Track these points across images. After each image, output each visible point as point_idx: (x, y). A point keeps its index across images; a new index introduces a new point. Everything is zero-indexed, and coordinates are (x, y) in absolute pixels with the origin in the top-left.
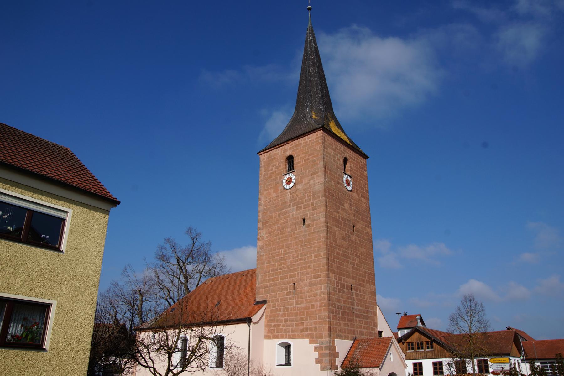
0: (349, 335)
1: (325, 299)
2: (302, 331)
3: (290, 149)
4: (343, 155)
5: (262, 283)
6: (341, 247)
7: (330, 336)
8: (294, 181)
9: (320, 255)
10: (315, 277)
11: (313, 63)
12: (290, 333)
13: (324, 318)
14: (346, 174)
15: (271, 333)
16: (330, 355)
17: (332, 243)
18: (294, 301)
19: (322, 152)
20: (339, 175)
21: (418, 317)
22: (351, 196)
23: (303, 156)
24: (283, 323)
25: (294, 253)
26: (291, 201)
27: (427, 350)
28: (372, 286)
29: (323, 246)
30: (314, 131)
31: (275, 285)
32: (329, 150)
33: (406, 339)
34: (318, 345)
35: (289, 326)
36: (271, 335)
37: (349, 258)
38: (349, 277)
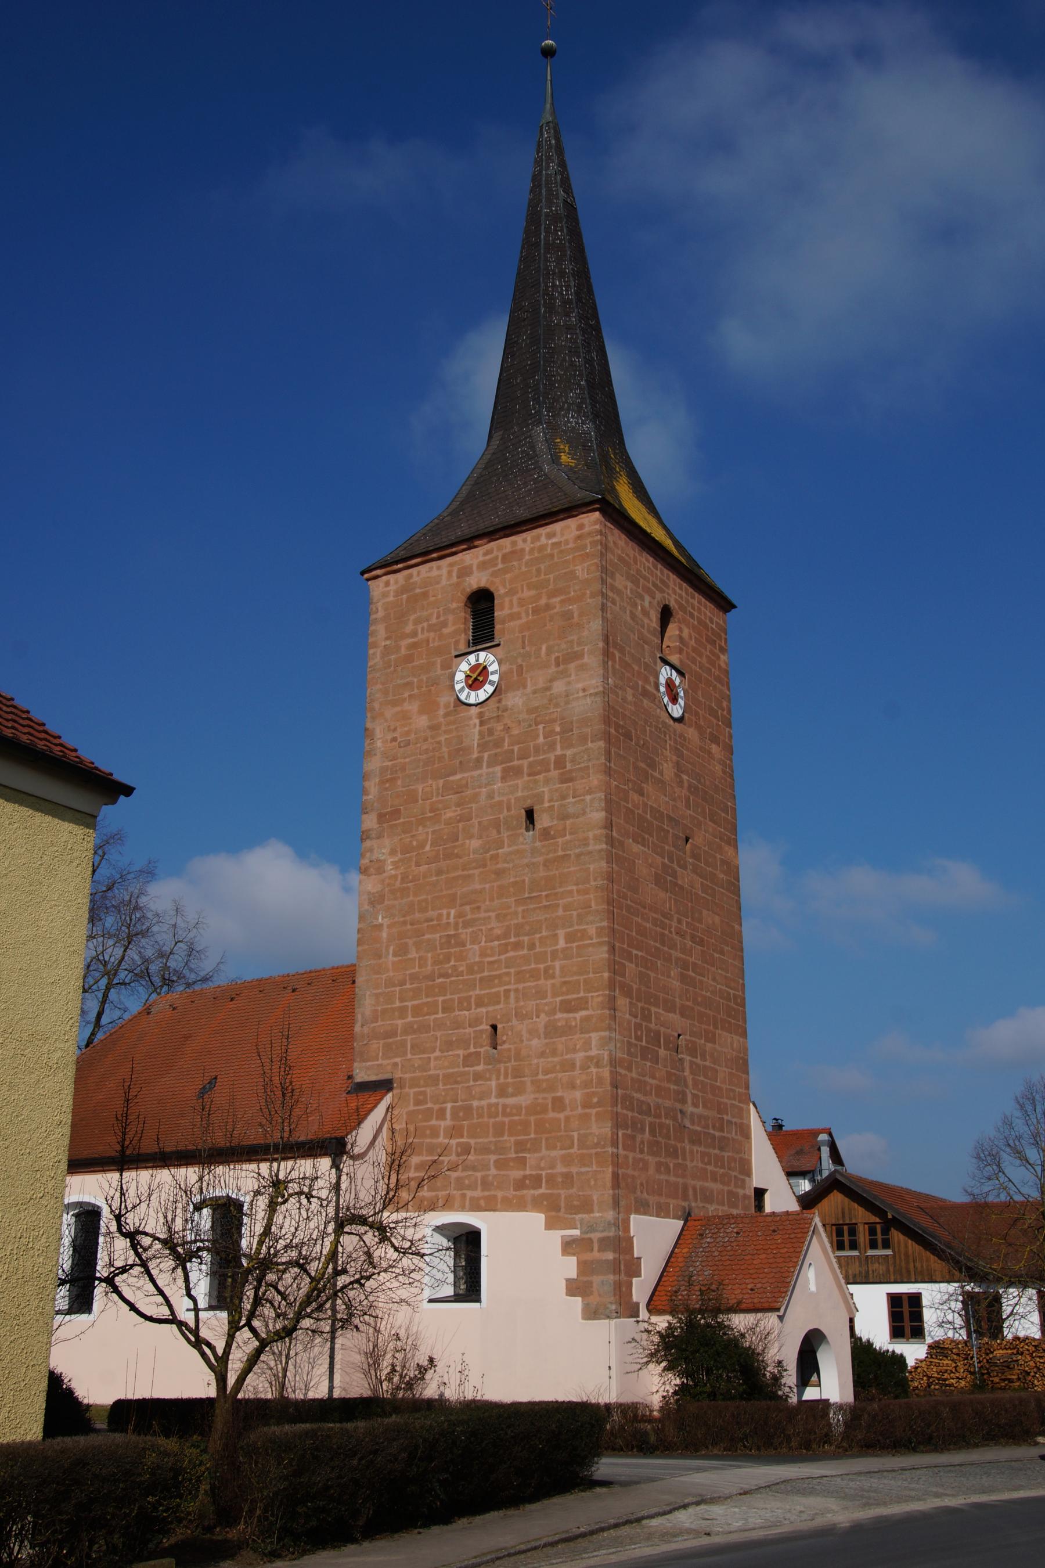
0: (672, 1202)
2: (520, 1185)
3: (483, 566)
4: (658, 596)
5: (375, 1019)
7: (616, 1203)
9: (584, 935)
10: (568, 1007)
11: (559, 261)
12: (478, 1193)
13: (597, 1145)
14: (666, 662)
16: (615, 1267)
18: (494, 1083)
19: (597, 586)
21: (823, 1137)
22: (681, 736)
23: (528, 594)
25: (494, 924)
26: (483, 747)
27: (870, 1253)
30: (570, 511)
31: (425, 1028)
32: (620, 582)
35: (474, 1168)
38: (671, 1009)
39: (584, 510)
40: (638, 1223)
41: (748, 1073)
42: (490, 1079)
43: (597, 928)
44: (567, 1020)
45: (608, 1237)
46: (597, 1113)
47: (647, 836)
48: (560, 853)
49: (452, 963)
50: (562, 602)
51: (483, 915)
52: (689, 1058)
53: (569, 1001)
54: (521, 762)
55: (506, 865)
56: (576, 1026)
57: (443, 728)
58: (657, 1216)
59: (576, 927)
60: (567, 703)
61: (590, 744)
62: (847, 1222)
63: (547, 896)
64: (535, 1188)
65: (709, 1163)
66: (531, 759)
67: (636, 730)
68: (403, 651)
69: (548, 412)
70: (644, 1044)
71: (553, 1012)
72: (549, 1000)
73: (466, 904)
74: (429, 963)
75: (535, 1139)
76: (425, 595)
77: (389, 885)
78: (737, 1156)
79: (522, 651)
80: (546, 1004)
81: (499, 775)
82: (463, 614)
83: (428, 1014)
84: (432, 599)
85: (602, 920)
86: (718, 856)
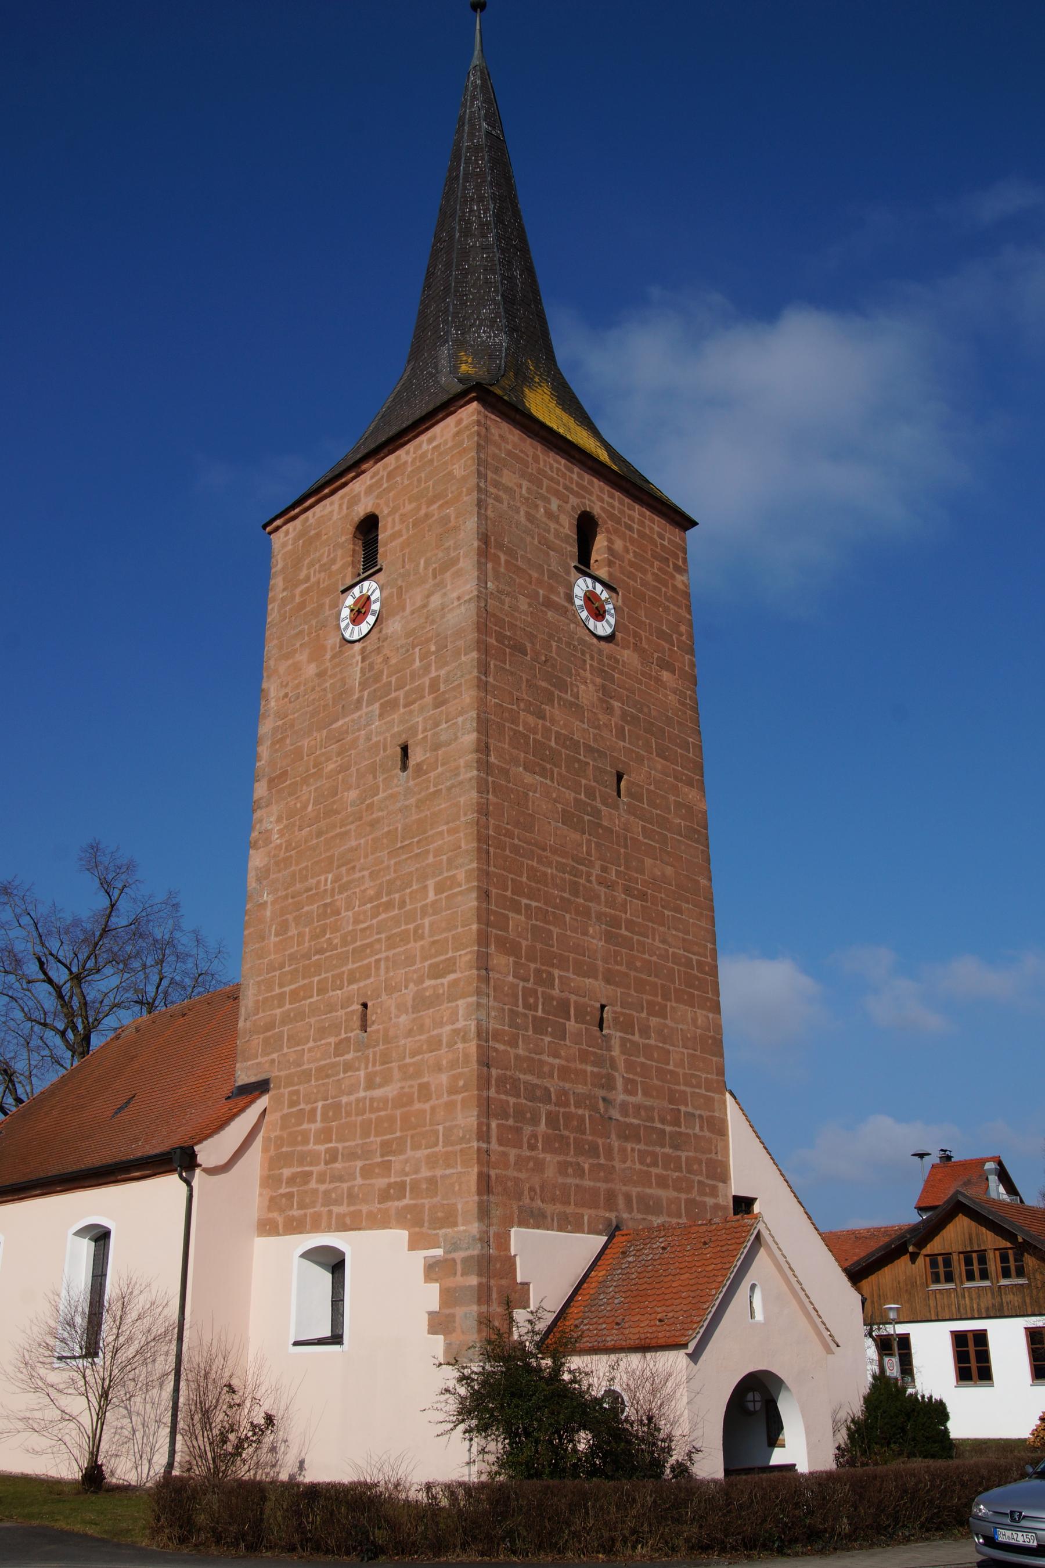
0: (587, 1214)
1: (466, 1056)
2: (385, 1196)
4: (573, 500)
6: (554, 851)
7: (484, 1213)
8: (376, 607)
9: (453, 881)
10: (437, 972)
11: (478, 187)
13: (462, 1140)
15: (281, 1210)
17: (509, 834)
18: (362, 1073)
19: (473, 481)
20: (553, 575)
21: (990, 1165)
23: (409, 507)
24: (322, 1167)
26: (364, 685)
27: (1004, 1282)
28: (702, 1015)
29: (468, 844)
31: (300, 1015)
32: (508, 478)
33: (921, 1244)
34: (439, 1252)
35: (341, 1179)
36: (280, 1220)
37: (596, 898)
39: (462, 402)
40: (522, 1241)
41: (722, 1056)
42: (358, 1069)
43: (466, 872)
44: (435, 987)
45: (472, 1257)
46: (463, 1100)
47: (548, 766)
48: (432, 790)
49: (328, 936)
50: (441, 507)
51: (357, 875)
52: (619, 1034)
53: (437, 965)
54: (397, 693)
55: (380, 814)
56: (443, 994)
57: (329, 673)
58: (560, 1229)
59: (446, 875)
60: (443, 617)
61: (463, 658)
62: (976, 1248)
63: (418, 842)
64: (399, 1199)
65: (655, 1164)
66: (407, 688)
67: (533, 644)
68: (298, 599)
69: (457, 330)
70: (540, 1013)
71: (420, 981)
72: (418, 966)
73: (343, 865)
74: (307, 938)
75: (400, 1138)
76: (318, 535)
77: (274, 856)
78: (704, 1157)
79: (402, 571)
80: (415, 971)
81: (377, 712)
82: (351, 546)
83: (305, 998)
84: (324, 537)
85: (471, 861)
86: (672, 798)
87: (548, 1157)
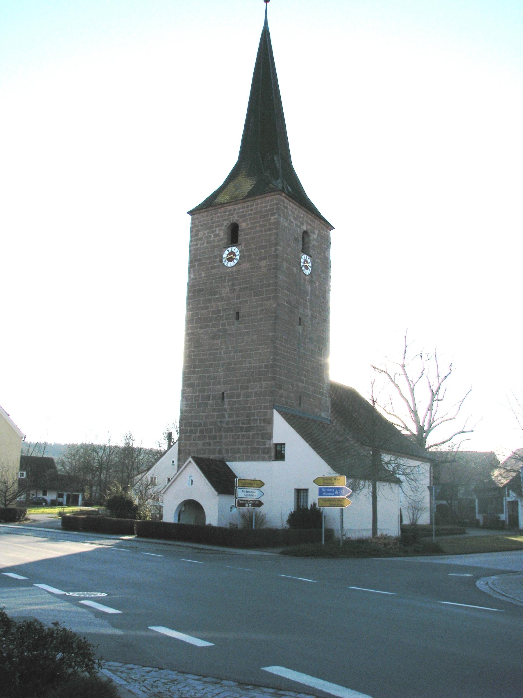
87: (199, 442)
